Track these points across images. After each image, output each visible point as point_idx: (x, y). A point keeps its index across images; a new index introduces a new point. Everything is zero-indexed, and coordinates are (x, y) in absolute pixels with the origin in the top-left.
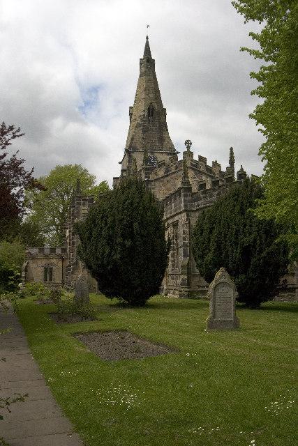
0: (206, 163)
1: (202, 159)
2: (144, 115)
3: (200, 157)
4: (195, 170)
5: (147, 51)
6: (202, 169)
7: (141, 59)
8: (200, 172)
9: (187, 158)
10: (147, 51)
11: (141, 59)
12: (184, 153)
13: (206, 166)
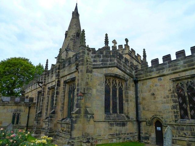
0: (135, 53)
1: (133, 51)
2: (74, 35)
3: (132, 49)
4: (130, 56)
5: (76, 9)
6: (134, 56)
7: (73, 12)
8: (133, 58)
9: (127, 48)
10: (76, 9)
11: (73, 12)
12: (125, 45)
13: (135, 55)
